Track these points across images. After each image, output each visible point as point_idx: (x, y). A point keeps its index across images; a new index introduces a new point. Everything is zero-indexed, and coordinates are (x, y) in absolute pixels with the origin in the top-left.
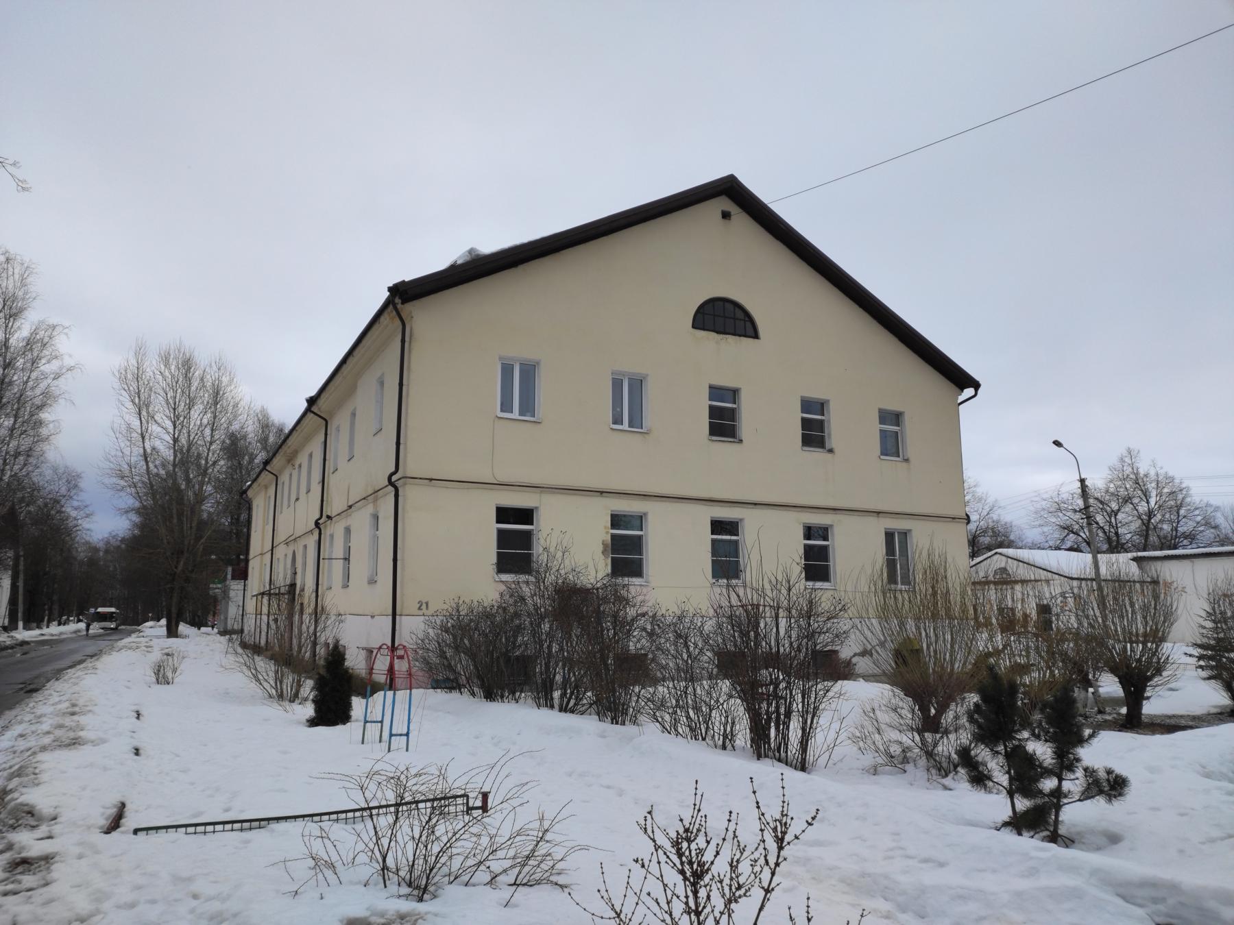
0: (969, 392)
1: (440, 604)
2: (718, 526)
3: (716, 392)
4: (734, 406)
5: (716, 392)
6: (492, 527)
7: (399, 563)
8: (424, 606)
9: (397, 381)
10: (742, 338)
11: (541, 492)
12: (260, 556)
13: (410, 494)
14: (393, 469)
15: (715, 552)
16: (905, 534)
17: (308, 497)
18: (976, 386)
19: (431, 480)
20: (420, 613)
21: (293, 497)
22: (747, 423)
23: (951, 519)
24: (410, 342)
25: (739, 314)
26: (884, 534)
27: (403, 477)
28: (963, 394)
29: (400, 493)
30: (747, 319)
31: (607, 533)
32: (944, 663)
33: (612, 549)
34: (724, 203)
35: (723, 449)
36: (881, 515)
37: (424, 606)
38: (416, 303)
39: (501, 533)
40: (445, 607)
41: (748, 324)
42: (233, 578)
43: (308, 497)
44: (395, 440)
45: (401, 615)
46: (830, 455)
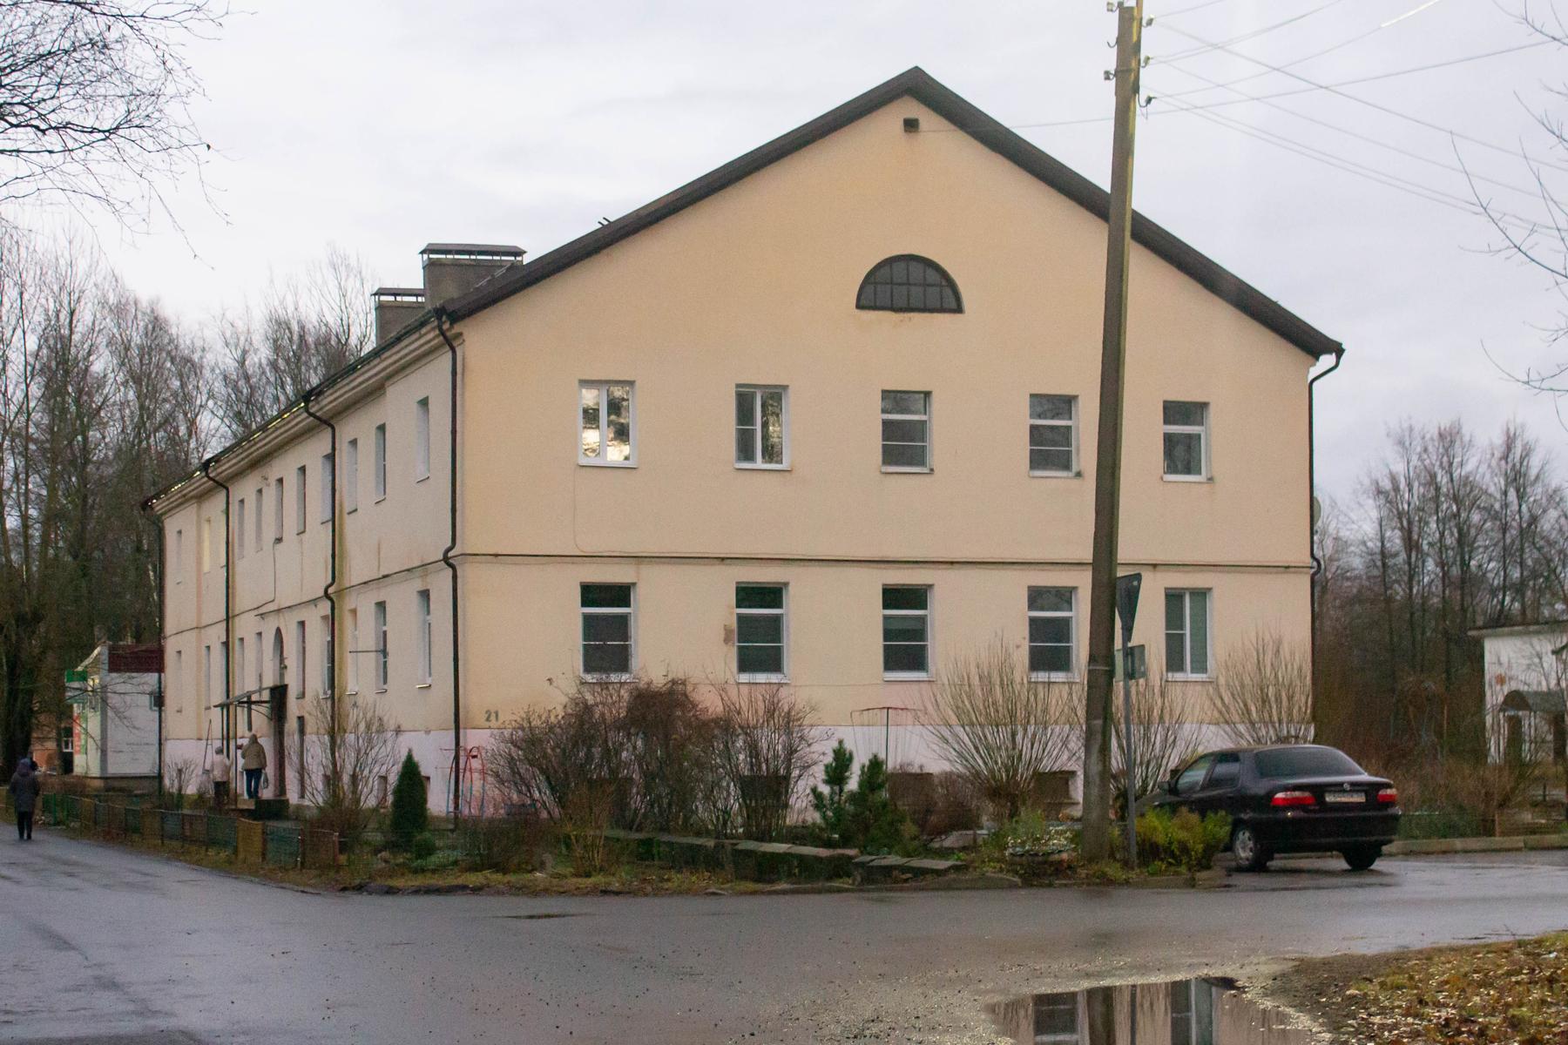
0: (1327, 360)
1: (510, 716)
2: (894, 596)
3: (894, 399)
4: (923, 418)
5: (894, 399)
6: (575, 612)
7: (460, 663)
8: (493, 718)
9: (449, 506)
10: (935, 315)
11: (639, 564)
12: (194, 633)
13: (468, 572)
14: (449, 544)
15: (888, 635)
16: (1201, 595)
17: (301, 542)
18: (1338, 350)
19: (496, 555)
20: (487, 724)
21: (269, 534)
22: (939, 444)
23: (1282, 569)
24: (463, 374)
25: (932, 276)
26: (1163, 597)
27: (462, 555)
28: (1318, 364)
29: (459, 574)
30: (944, 283)
31: (732, 613)
32: (1018, 764)
33: (739, 634)
34: (911, 108)
35: (905, 485)
36: (1158, 568)
37: (493, 715)
38: (467, 321)
39: (588, 619)
40: (515, 717)
41: (948, 292)
42: (1066, 777)
43: (301, 542)
44: (452, 655)
45: (465, 728)
46: (1077, 482)
